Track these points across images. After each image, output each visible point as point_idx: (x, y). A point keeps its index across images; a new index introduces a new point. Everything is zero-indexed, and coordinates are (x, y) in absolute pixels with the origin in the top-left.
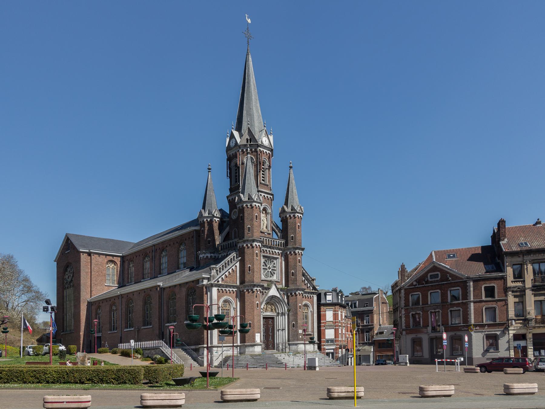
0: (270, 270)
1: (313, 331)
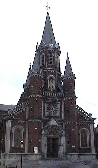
0: (53, 110)
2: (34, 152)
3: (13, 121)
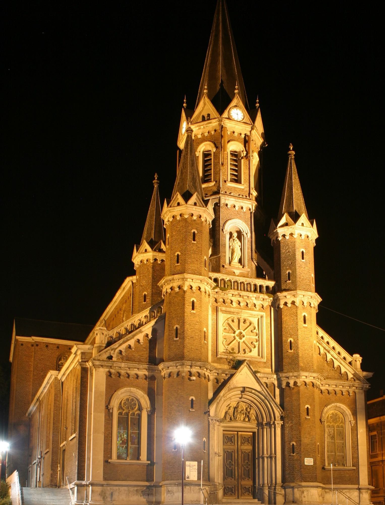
1: (356, 464)
2: (188, 477)
3: (112, 371)
